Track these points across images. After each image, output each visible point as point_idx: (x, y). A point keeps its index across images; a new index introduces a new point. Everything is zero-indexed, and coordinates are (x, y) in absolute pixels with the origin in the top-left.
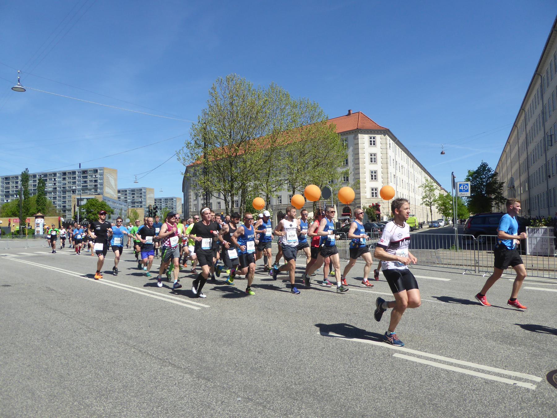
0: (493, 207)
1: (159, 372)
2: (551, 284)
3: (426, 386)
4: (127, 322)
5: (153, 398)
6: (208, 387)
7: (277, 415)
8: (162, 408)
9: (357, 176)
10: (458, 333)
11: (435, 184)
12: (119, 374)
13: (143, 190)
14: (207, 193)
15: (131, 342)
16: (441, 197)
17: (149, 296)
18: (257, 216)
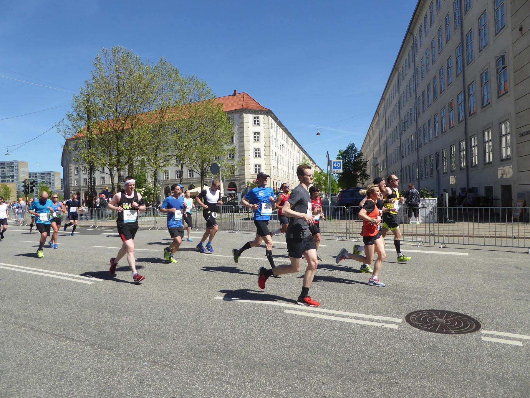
0: (358, 182)
1: (56, 347)
2: (405, 246)
3: (314, 335)
4: (11, 301)
5: (54, 373)
6: (111, 356)
7: (184, 374)
8: (65, 381)
9: (241, 154)
10: (336, 289)
11: (311, 162)
12: (10, 354)
13: (15, 164)
14: (91, 167)
15: (19, 321)
16: (316, 173)
17: (33, 274)
18: (145, 191)
